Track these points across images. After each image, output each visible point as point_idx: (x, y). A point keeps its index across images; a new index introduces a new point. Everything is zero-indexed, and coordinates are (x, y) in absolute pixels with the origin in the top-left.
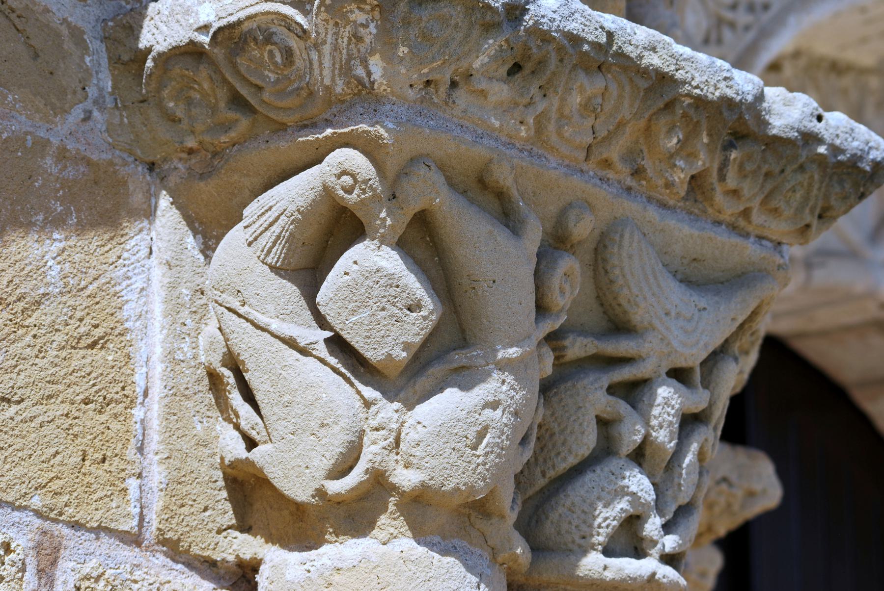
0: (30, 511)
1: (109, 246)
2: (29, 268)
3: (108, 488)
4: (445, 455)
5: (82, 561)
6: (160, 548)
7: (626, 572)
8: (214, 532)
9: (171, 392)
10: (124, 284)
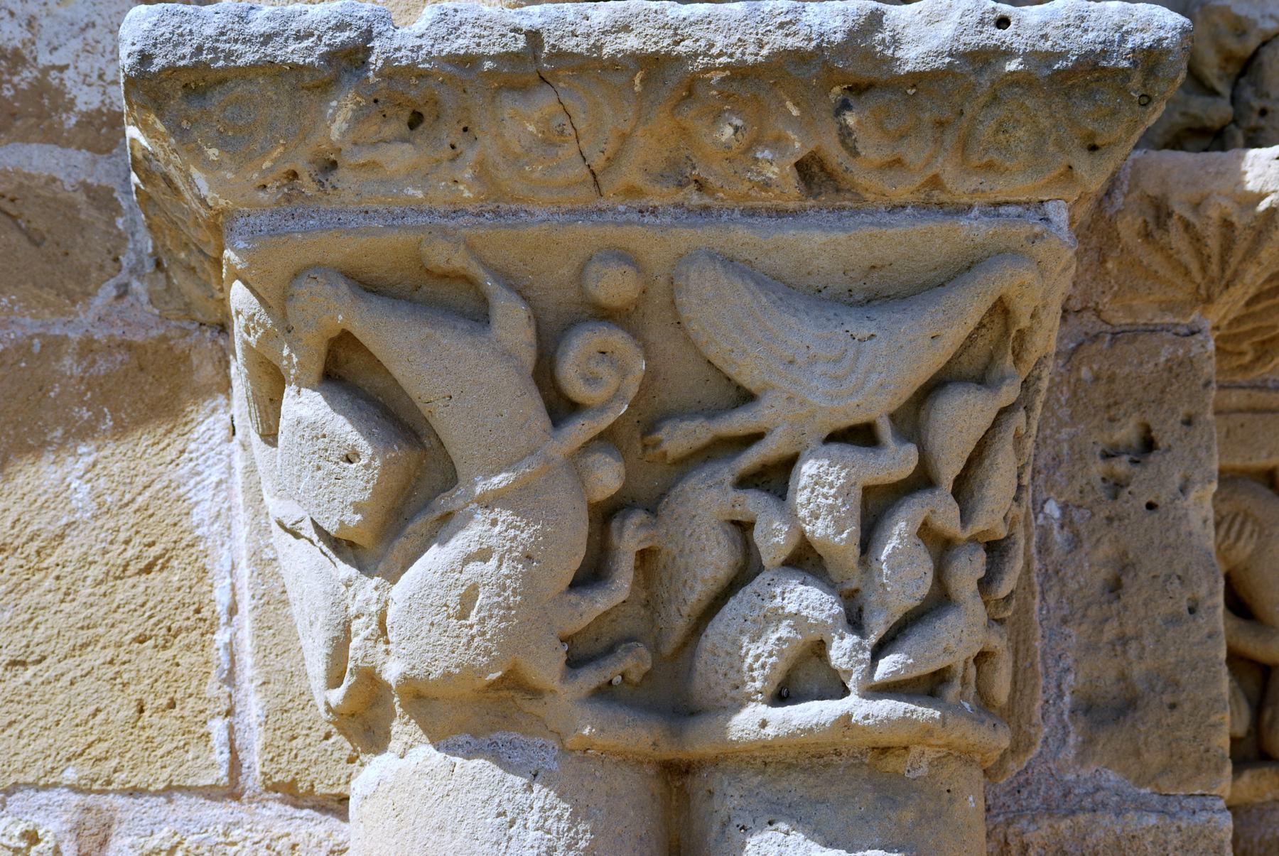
0: (63, 787)
1: (167, 441)
2: (43, 498)
3: (179, 737)
4: (423, 634)
5: (149, 832)
6: (273, 795)
7: (794, 723)
8: (343, 762)
9: (262, 601)
10: (192, 483)
